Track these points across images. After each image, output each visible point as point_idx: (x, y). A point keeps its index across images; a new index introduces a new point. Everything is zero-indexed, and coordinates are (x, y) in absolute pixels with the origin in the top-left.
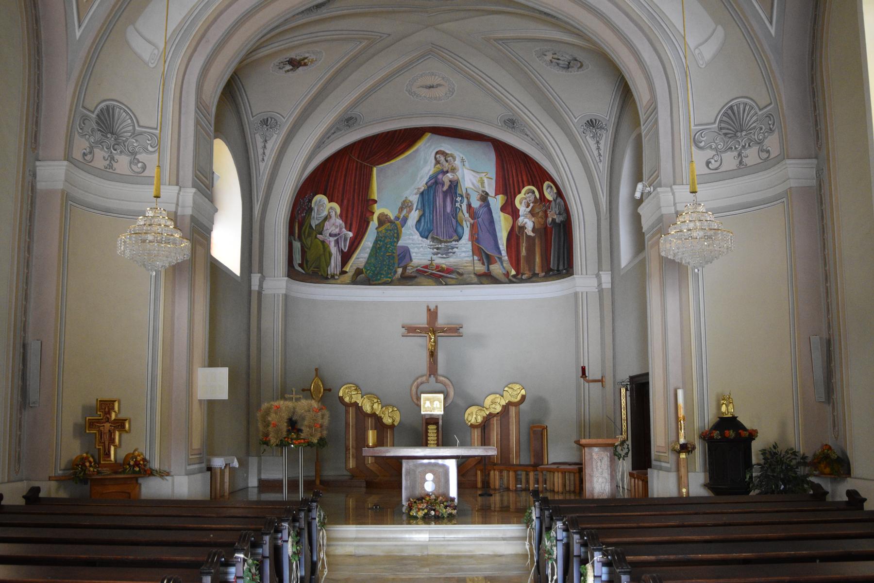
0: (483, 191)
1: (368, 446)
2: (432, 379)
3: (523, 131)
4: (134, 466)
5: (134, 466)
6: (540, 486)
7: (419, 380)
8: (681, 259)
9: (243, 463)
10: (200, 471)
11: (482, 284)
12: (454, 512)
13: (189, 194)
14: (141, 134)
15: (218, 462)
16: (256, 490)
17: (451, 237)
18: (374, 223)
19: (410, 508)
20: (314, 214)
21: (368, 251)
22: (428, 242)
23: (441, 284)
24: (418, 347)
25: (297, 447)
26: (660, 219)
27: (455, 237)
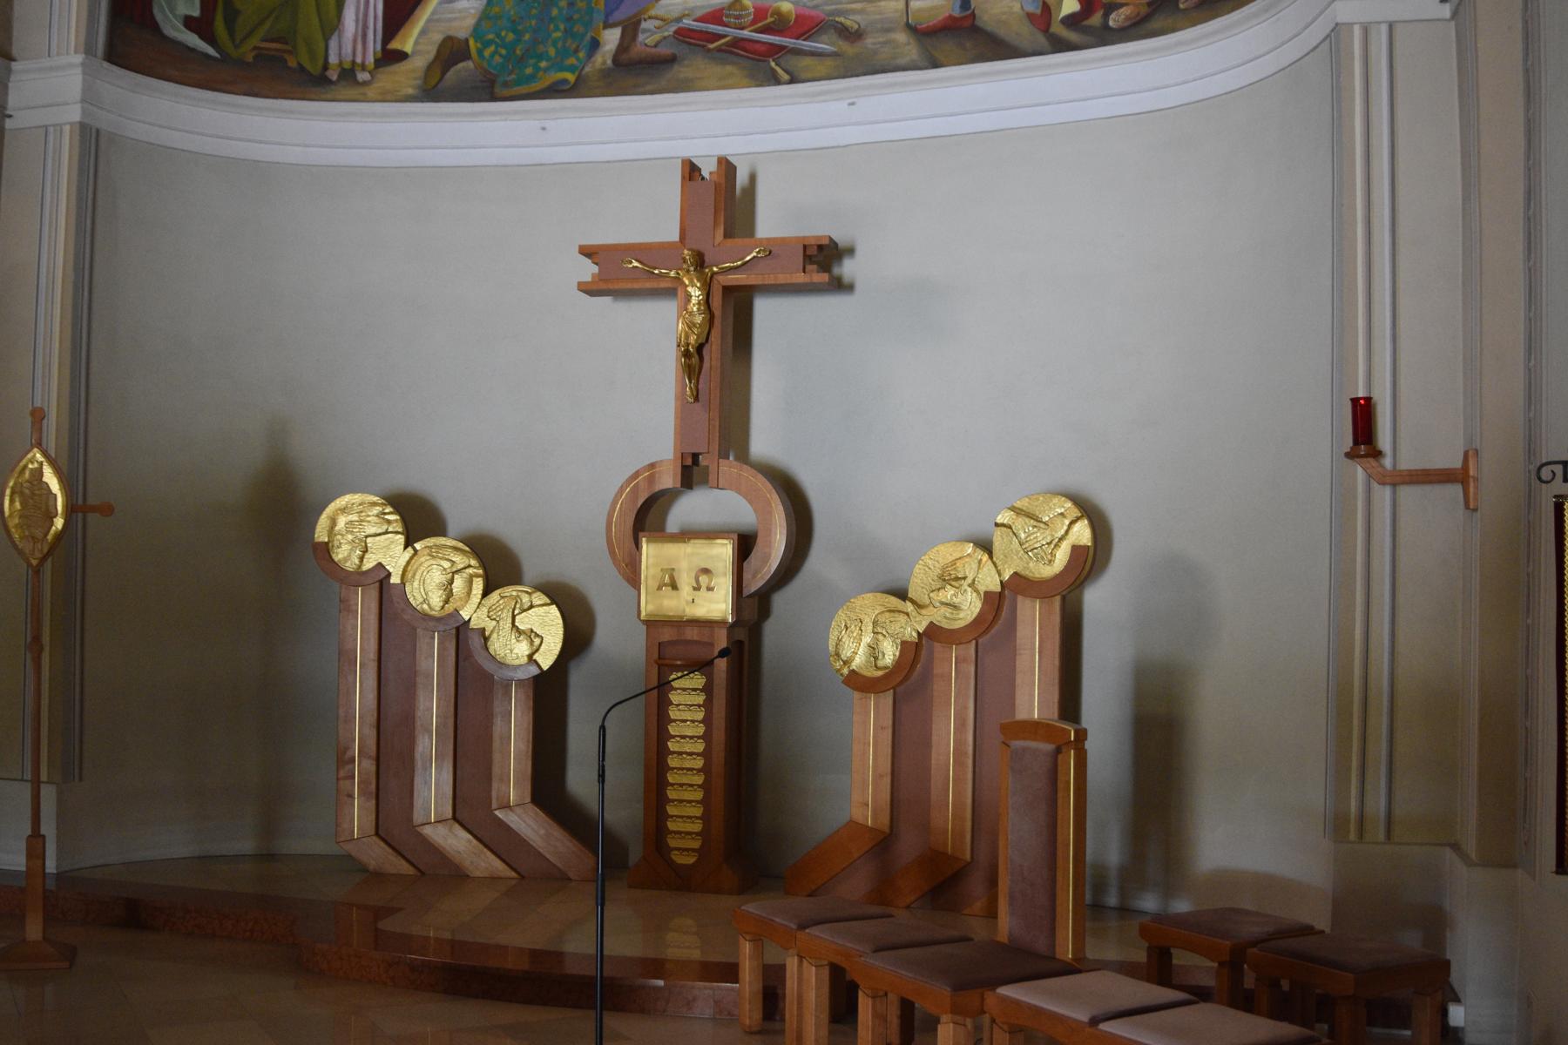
11: (935, 65)
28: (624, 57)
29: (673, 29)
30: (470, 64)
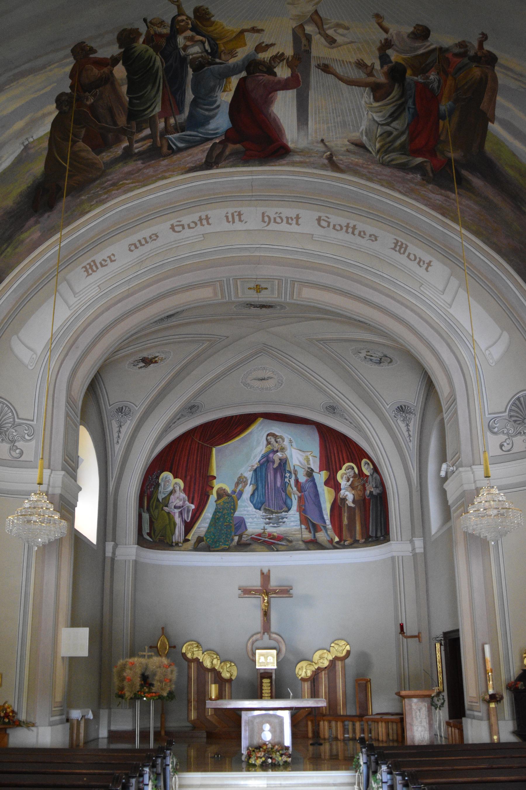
0: (309, 468)
1: (211, 699)
2: (266, 636)
3: (342, 416)
4: (4, 717)
5: (4, 717)
6: (365, 736)
7: (254, 638)
8: (480, 533)
9: (96, 716)
10: (61, 722)
11: (309, 549)
12: (289, 760)
13: (59, 476)
14: (20, 425)
15: (76, 714)
16: (106, 741)
17: (282, 509)
18: (213, 496)
19: (249, 756)
20: (161, 489)
21: (208, 521)
22: (261, 513)
23: (273, 550)
24: (252, 607)
25: (149, 699)
26: (463, 494)
27: (285, 509)
28: (239, 543)
29: (250, 537)
30: (204, 543)
